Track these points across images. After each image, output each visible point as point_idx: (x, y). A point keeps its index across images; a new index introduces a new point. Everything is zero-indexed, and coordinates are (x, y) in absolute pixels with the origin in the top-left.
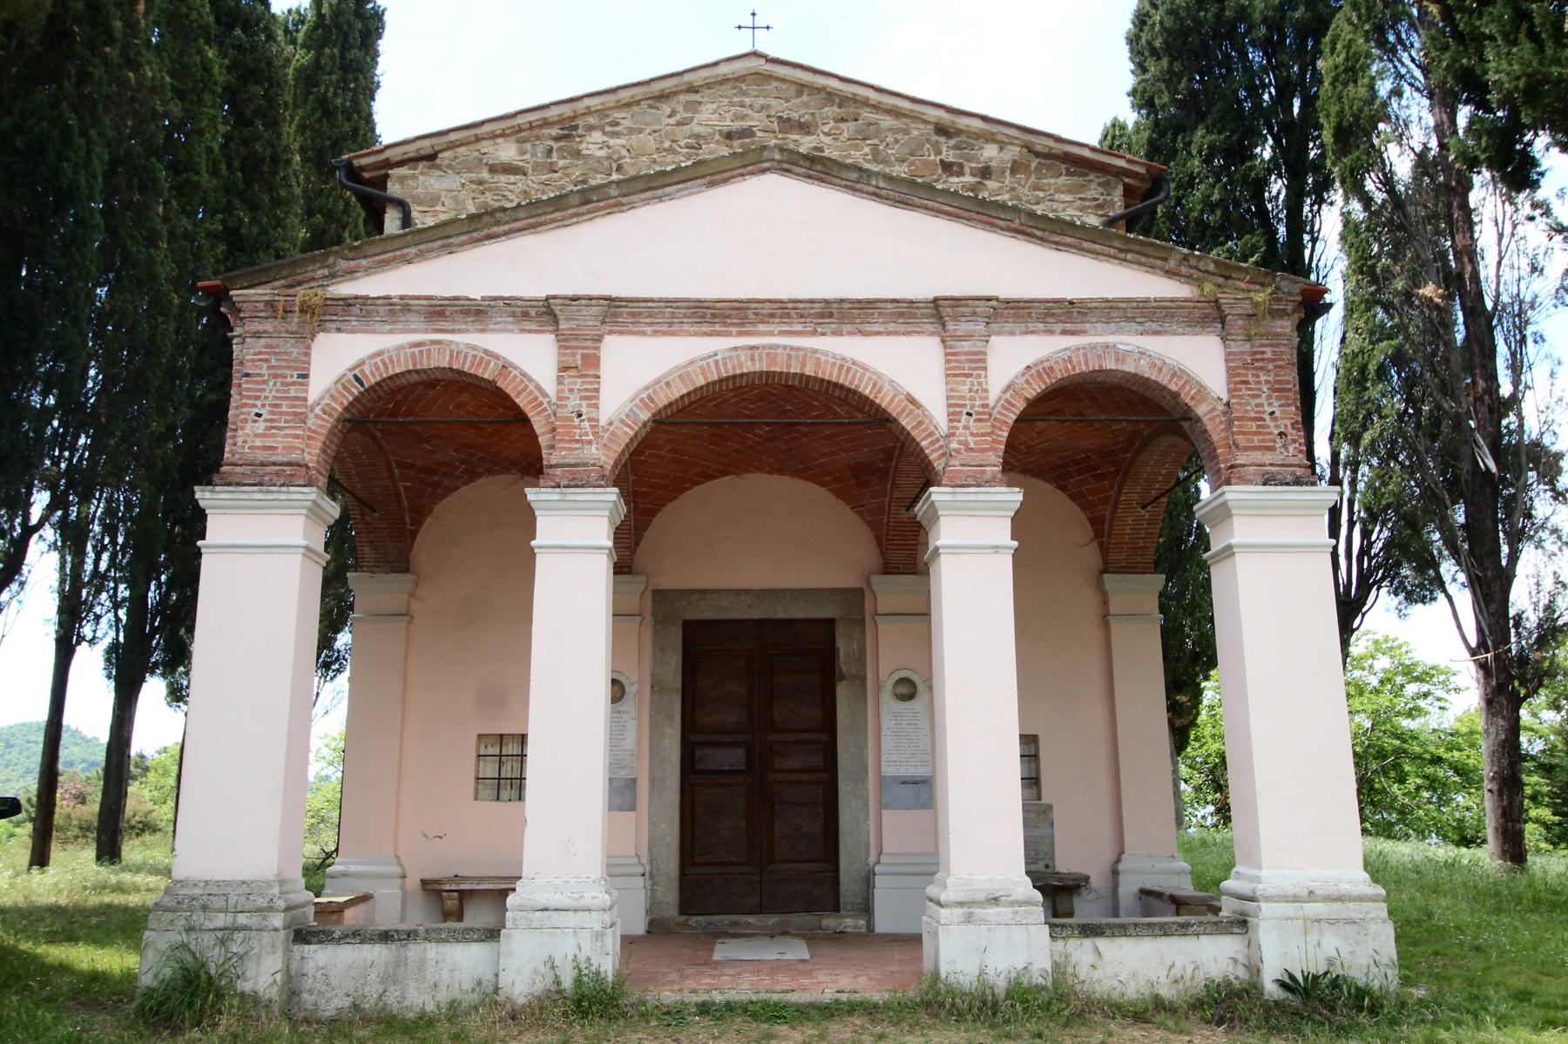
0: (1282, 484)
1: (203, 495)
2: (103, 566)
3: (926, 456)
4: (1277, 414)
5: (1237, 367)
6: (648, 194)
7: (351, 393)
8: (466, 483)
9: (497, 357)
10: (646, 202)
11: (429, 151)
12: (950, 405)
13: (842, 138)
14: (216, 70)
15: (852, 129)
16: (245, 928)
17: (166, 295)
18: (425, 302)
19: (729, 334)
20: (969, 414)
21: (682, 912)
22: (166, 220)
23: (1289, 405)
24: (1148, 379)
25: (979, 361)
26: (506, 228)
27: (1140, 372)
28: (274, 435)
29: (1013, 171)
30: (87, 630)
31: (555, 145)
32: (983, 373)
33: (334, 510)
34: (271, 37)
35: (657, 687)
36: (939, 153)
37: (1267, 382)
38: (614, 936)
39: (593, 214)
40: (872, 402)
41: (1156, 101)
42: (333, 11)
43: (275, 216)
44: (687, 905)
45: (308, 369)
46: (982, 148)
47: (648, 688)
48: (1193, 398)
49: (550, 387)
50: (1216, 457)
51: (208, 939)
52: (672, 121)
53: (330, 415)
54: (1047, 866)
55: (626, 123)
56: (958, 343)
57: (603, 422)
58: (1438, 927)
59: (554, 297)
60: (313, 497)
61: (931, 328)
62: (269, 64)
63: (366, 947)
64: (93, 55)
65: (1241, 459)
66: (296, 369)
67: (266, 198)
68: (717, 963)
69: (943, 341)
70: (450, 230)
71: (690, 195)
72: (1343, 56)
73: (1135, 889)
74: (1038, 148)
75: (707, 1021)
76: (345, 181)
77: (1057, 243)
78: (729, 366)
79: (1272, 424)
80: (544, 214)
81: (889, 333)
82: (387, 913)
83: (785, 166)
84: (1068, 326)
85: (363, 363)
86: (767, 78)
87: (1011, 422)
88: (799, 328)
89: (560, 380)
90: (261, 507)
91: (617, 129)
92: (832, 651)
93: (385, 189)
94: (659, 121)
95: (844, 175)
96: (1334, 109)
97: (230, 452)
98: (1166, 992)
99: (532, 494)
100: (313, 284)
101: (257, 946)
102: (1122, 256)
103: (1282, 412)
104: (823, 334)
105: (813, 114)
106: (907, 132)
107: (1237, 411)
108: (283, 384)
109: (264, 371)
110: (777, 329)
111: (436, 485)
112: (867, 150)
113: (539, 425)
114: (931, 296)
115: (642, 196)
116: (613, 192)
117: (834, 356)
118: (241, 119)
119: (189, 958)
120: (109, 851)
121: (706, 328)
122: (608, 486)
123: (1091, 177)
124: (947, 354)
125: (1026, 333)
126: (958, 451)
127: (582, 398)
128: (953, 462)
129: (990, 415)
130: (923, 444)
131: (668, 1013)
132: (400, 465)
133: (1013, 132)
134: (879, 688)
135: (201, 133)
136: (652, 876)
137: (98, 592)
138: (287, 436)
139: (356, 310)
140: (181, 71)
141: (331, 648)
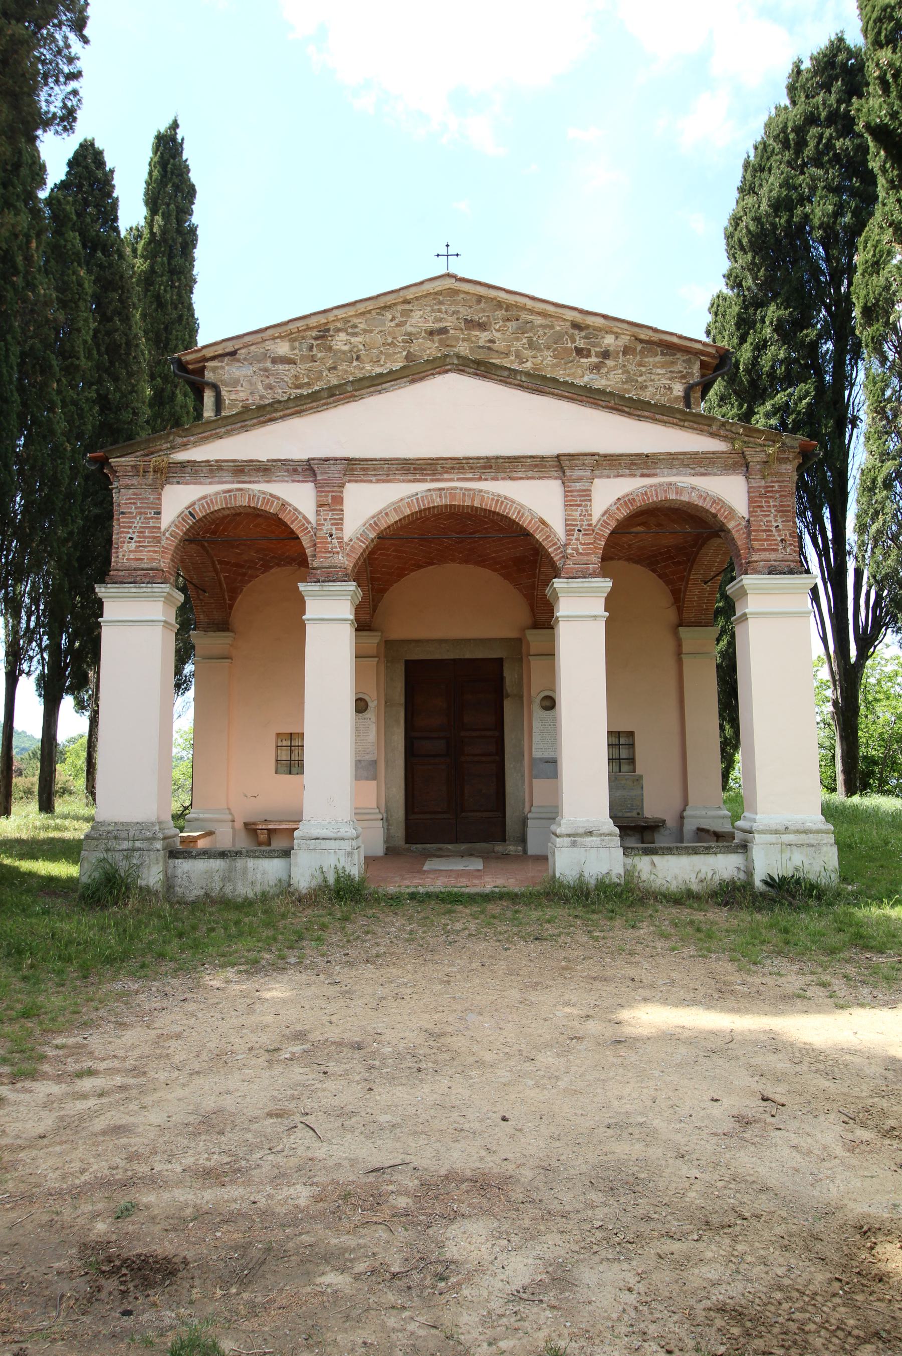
0: (780, 573)
1: (100, 590)
2: (32, 624)
3: (552, 558)
4: (781, 527)
5: (756, 497)
6: (372, 389)
7: (188, 524)
8: (262, 573)
9: (278, 498)
10: (371, 394)
11: (230, 349)
12: (567, 525)
13: (508, 333)
14: (86, 285)
15: (514, 327)
16: (140, 849)
17: (62, 445)
18: (232, 464)
19: (425, 481)
20: (579, 531)
21: (407, 842)
22: (59, 392)
23: (788, 521)
24: (697, 505)
25: (586, 495)
26: (281, 414)
27: (692, 501)
28: (141, 551)
29: (625, 353)
30: (25, 666)
31: (315, 343)
32: (589, 503)
33: (180, 597)
34: (121, 256)
35: (389, 703)
36: (574, 341)
37: (775, 506)
38: (359, 855)
39: (337, 403)
40: (518, 524)
41: (744, 283)
42: (161, 230)
43: (131, 383)
44: (410, 837)
45: (160, 508)
46: (603, 338)
47: (383, 702)
48: (726, 517)
49: (312, 517)
50: (740, 555)
51: (119, 856)
52: (393, 324)
53: (175, 538)
54: (638, 814)
55: (361, 326)
56: (573, 484)
57: (346, 539)
58: (890, 851)
59: (313, 459)
60: (168, 590)
61: (555, 474)
62: (122, 277)
63: (211, 860)
64: (6, 283)
65: (755, 557)
66: (153, 508)
67: (124, 372)
68: (425, 871)
69: (563, 483)
70: (246, 416)
71: (399, 388)
72: (872, 253)
73: (694, 828)
74: (642, 337)
75: (414, 903)
76: (177, 371)
77: (638, 416)
78: (426, 502)
79: (776, 534)
80: (305, 404)
81: (528, 478)
82: (225, 839)
83: (461, 368)
84: (645, 471)
85: (194, 503)
86: (455, 292)
87: (606, 535)
88: (471, 476)
89: (318, 513)
90: (136, 597)
91: (356, 330)
92: (501, 678)
93: (203, 375)
94: (384, 325)
95: (499, 373)
96: (863, 293)
97: (116, 562)
98: (695, 887)
99: (302, 587)
100: (161, 453)
101: (147, 860)
102: (682, 423)
103: (783, 526)
104: (486, 480)
105: (488, 316)
106: (551, 327)
107: (754, 525)
108: (145, 518)
109: (133, 510)
110: (456, 477)
111: (244, 574)
112: (525, 341)
113: (305, 542)
114: (556, 452)
115: (368, 390)
116: (349, 388)
117: (493, 494)
118: (105, 318)
119: (108, 867)
120: (46, 806)
121: (410, 477)
122: (350, 581)
123: (679, 355)
124: (565, 492)
125: (618, 476)
126: (571, 555)
127: (332, 524)
128: (569, 562)
129: (593, 531)
130: (550, 550)
131: (392, 899)
132: (220, 562)
133: (625, 326)
134: (530, 702)
135: (79, 330)
136: (387, 820)
137: (30, 642)
138: (149, 551)
139: (188, 469)
140: (63, 288)
141: (181, 675)
